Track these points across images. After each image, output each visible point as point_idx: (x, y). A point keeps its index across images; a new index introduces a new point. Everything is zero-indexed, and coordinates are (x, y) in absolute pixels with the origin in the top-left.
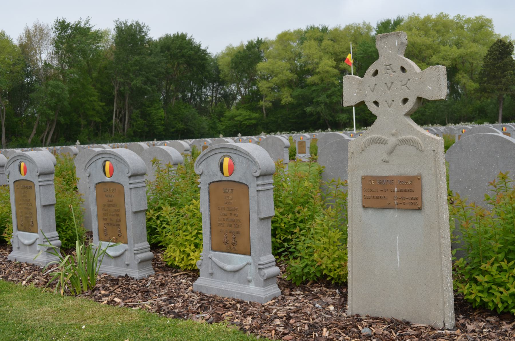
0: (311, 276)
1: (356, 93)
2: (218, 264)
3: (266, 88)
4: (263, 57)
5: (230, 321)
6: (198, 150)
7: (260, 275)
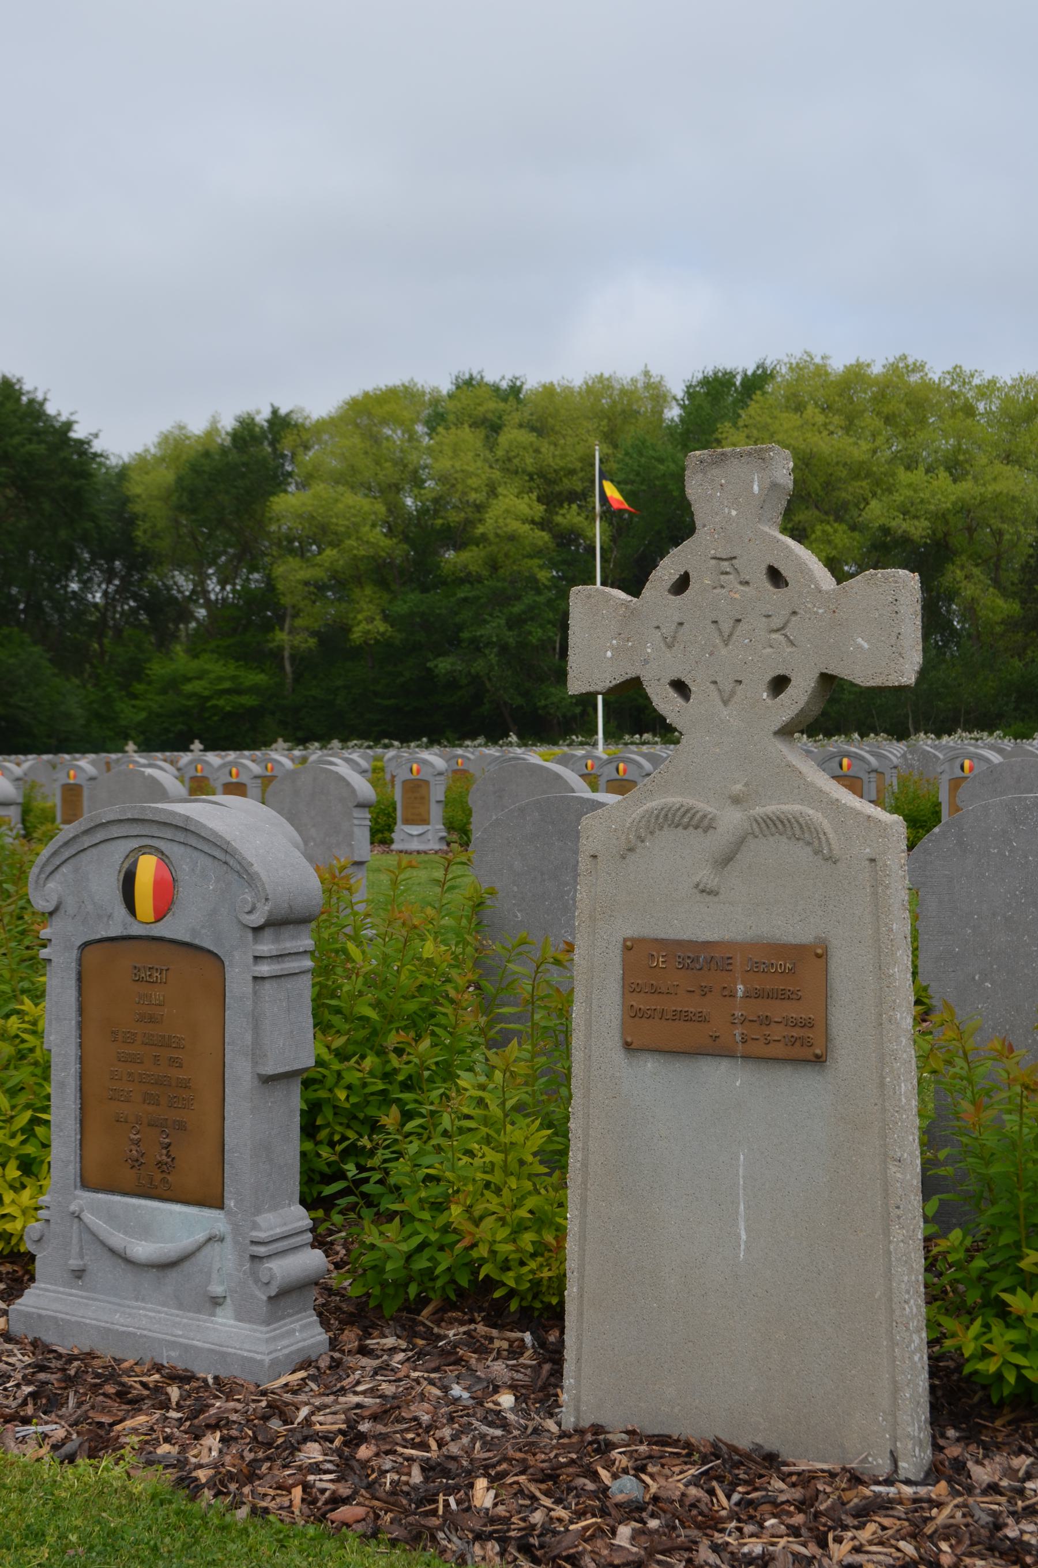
0: (439, 1283)
1: (613, 649)
2: (103, 1235)
3: (298, 581)
4: (290, 474)
5: (141, 1449)
6: (45, 798)
7: (257, 1281)
